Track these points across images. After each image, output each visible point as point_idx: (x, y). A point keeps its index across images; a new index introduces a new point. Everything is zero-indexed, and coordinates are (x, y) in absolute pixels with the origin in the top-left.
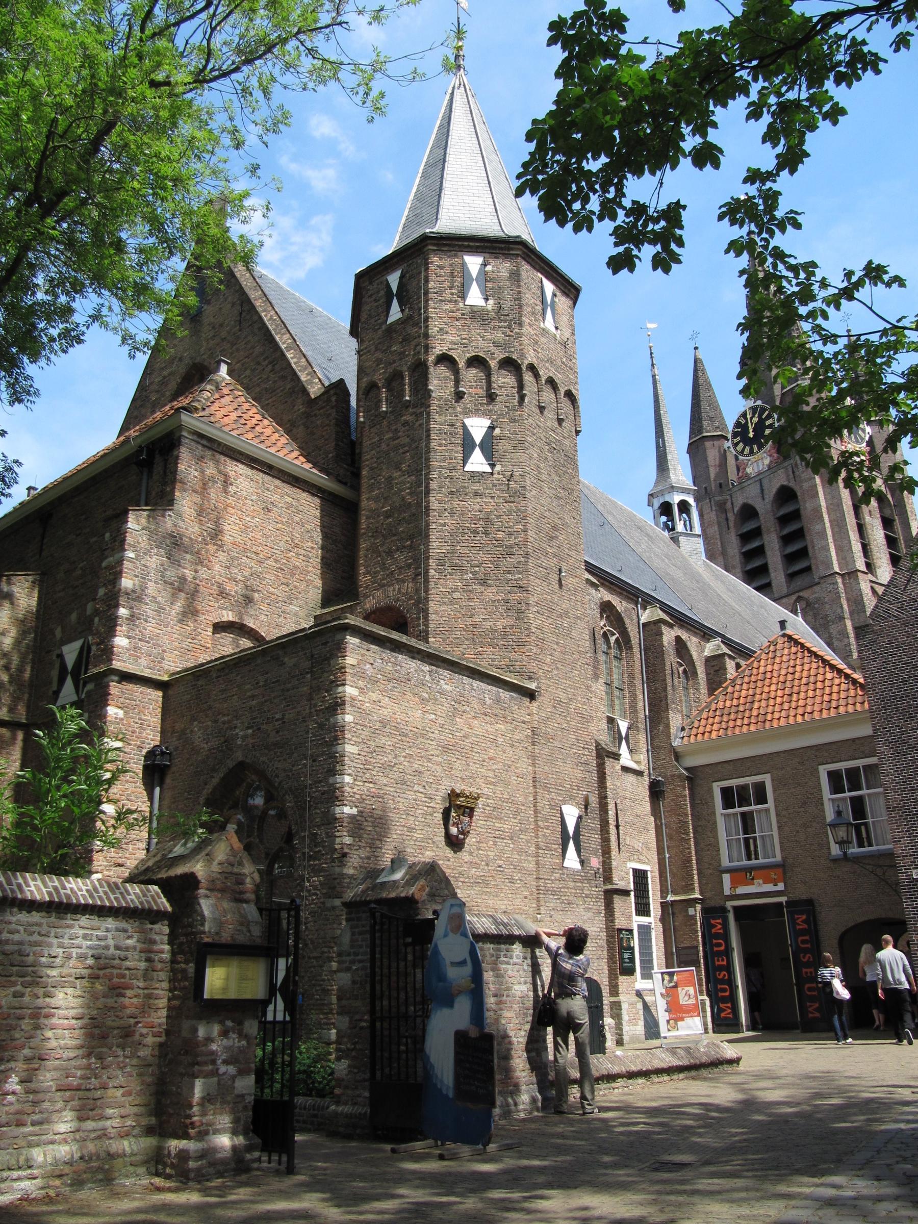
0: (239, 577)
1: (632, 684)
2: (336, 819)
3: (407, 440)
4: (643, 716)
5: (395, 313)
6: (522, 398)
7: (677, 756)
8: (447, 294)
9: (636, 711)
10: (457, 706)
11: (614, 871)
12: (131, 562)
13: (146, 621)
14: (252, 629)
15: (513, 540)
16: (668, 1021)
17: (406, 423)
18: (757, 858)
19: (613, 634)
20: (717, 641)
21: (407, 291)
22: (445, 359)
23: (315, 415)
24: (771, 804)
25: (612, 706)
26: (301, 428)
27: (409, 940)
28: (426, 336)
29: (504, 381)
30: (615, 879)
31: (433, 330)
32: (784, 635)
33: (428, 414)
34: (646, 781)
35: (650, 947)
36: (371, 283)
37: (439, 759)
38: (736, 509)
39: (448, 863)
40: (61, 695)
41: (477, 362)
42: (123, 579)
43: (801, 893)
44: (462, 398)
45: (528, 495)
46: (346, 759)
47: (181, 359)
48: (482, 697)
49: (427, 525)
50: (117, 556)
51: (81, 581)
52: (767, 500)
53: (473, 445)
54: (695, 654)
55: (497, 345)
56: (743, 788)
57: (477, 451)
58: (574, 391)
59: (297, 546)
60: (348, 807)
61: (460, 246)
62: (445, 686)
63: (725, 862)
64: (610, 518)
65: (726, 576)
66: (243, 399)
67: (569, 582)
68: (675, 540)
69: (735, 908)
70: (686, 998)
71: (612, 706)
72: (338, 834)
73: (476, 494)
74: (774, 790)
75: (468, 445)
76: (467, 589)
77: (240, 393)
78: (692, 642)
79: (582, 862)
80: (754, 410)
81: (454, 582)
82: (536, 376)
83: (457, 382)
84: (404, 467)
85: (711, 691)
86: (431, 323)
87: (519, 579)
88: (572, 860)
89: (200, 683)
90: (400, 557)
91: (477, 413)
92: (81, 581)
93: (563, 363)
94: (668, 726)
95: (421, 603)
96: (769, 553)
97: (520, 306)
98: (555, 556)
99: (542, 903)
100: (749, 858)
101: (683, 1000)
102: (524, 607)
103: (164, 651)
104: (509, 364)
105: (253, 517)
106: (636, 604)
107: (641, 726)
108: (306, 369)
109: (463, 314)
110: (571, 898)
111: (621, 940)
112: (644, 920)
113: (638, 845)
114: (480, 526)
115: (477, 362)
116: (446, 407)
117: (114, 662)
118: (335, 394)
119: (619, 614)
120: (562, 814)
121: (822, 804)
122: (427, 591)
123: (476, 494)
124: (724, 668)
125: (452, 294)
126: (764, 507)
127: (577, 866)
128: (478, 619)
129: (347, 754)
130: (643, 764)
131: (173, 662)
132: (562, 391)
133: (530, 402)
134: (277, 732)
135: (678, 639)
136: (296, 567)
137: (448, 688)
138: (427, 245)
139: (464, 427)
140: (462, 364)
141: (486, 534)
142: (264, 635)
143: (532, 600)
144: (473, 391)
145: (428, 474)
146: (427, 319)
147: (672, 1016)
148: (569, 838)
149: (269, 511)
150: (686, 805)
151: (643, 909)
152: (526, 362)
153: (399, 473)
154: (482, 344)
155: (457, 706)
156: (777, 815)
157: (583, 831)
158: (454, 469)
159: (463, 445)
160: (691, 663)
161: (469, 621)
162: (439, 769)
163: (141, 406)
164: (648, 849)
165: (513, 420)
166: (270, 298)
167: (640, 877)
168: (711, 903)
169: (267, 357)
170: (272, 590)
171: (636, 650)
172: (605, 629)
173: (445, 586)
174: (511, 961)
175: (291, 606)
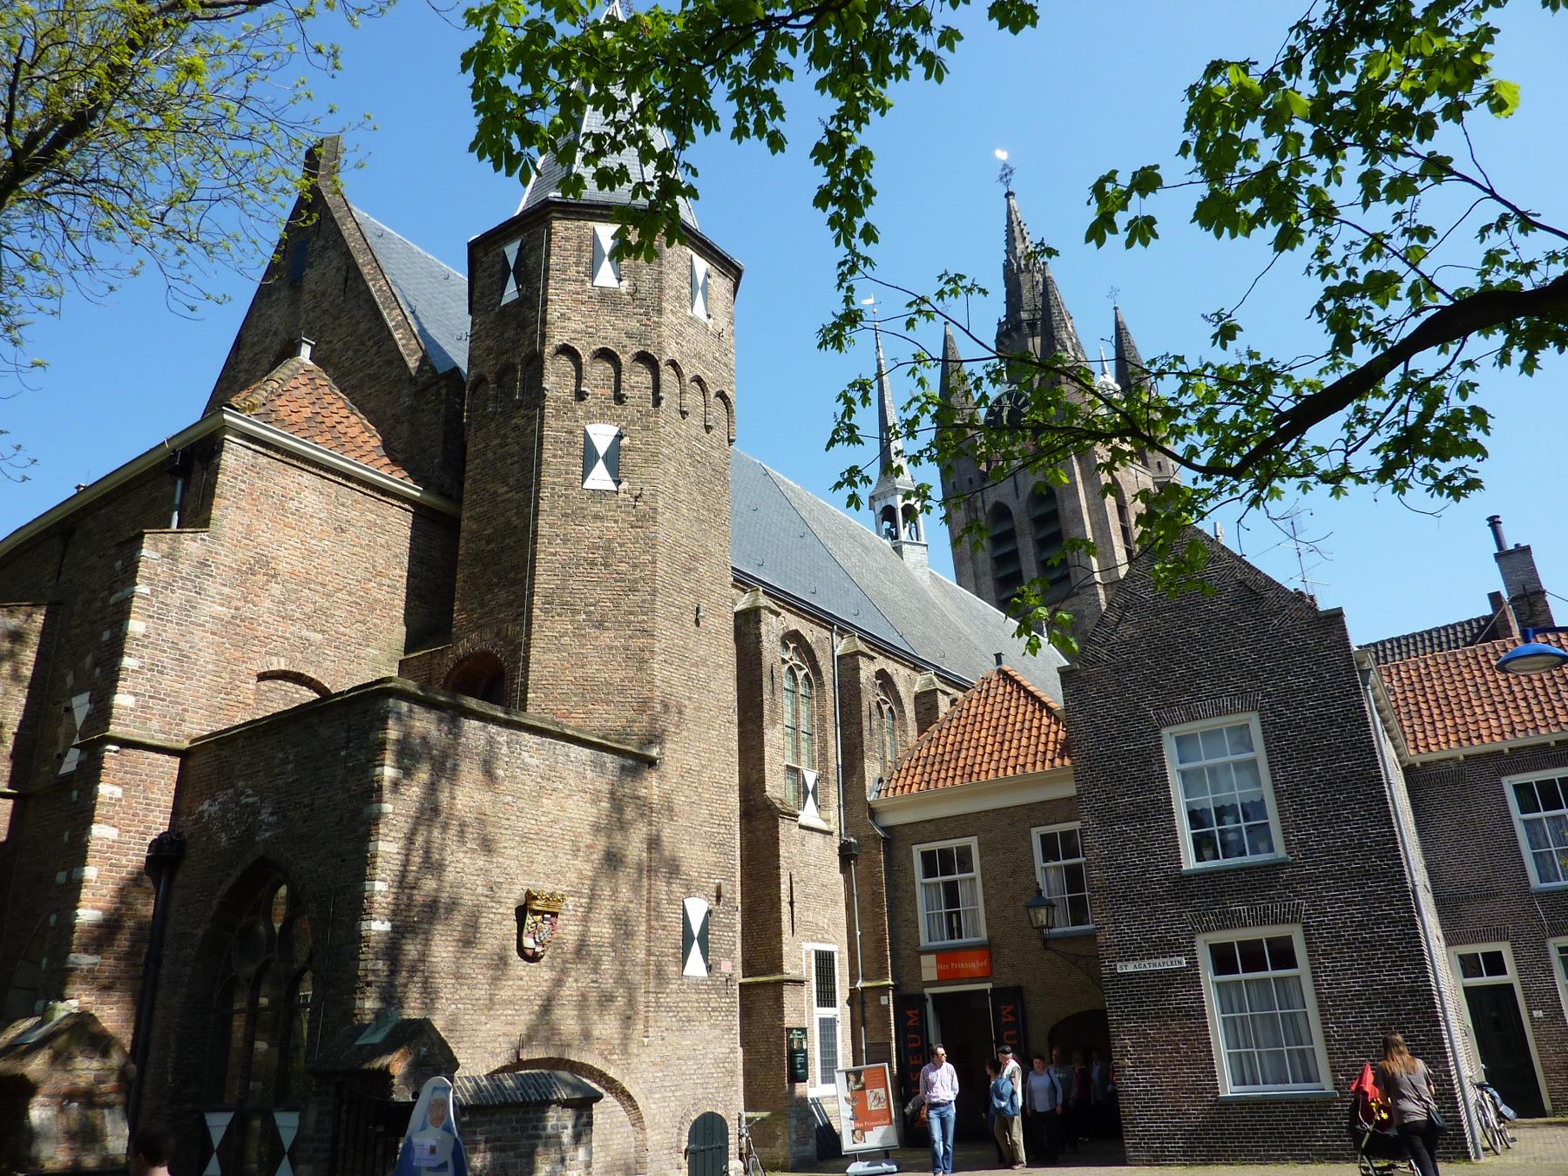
0: (297, 615)
1: (822, 729)
2: (361, 937)
3: (517, 448)
4: (834, 766)
5: (511, 292)
6: (657, 401)
7: (873, 813)
8: (572, 272)
9: (826, 760)
10: (544, 783)
11: (785, 958)
12: (144, 598)
13: (162, 673)
14: (312, 679)
15: (638, 574)
16: (853, 1132)
17: (517, 427)
18: (960, 937)
19: (801, 669)
20: (931, 674)
21: (525, 266)
22: (567, 351)
23: (423, 411)
24: (977, 872)
25: (797, 754)
26: (406, 425)
27: (380, 1129)
28: (544, 322)
29: (637, 380)
30: (786, 968)
31: (553, 313)
32: (1000, 671)
33: (542, 418)
34: (837, 842)
35: (835, 1045)
36: (486, 254)
37: (515, 852)
38: (987, 509)
39: (520, 983)
40: (66, 760)
41: (605, 355)
42: (131, 622)
43: (1008, 979)
44: (584, 399)
45: (659, 518)
46: (379, 860)
47: (275, 333)
48: (581, 770)
49: (534, 554)
50: (127, 591)
51: (99, 616)
52: (1021, 499)
53: (606, 459)
54: (902, 689)
55: (630, 336)
56: (945, 853)
57: (600, 465)
58: (728, 393)
59: (380, 574)
60: (378, 922)
61: (590, 214)
62: (528, 760)
63: (924, 941)
64: (815, 527)
65: (958, 591)
66: (327, 390)
67: (709, 622)
68: (898, 550)
69: (934, 996)
70: (876, 1102)
71: (797, 754)
72: (362, 957)
73: (596, 517)
74: (981, 857)
75: (589, 457)
76: (578, 634)
77: (324, 383)
78: (899, 673)
79: (709, 968)
80: (1009, 395)
81: (564, 625)
82: (679, 374)
83: (579, 379)
84: (511, 481)
85: (922, 730)
86: (550, 308)
87: (644, 621)
88: (696, 965)
89: (224, 753)
90: (503, 595)
91: (602, 418)
92: (99, 616)
93: (715, 358)
94: (863, 777)
95: (519, 650)
96: (1023, 558)
97: (661, 289)
98: (691, 591)
99: (651, 1023)
100: (952, 938)
101: (872, 1105)
102: (647, 655)
103: (185, 710)
104: (645, 358)
105: (321, 540)
106: (831, 631)
107: (832, 777)
108: (415, 353)
109: (590, 297)
110: (692, 1014)
111: (791, 1041)
112: (827, 1012)
113: (823, 922)
114: (598, 556)
115: (605, 355)
116: (563, 410)
117: (111, 727)
118: (446, 385)
119: (809, 646)
120: (684, 910)
121: (1034, 874)
122: (529, 634)
123: (596, 517)
124: (934, 707)
125: (578, 272)
126: (1017, 506)
127: (703, 972)
128: (590, 670)
129: (380, 853)
130: (833, 822)
131: (198, 724)
132: (712, 393)
133: (668, 407)
134: (305, 821)
135: (882, 674)
136: (377, 601)
137: (534, 762)
138: (550, 212)
139: (586, 435)
140: (585, 358)
141: (606, 565)
142: (327, 685)
143: (657, 647)
144: (599, 391)
145: (538, 492)
146: (545, 302)
147: (858, 1125)
148: (693, 939)
149: (343, 531)
150: (880, 872)
151: (826, 997)
152: (665, 358)
153: (506, 489)
154: (612, 334)
155: (544, 783)
156: (984, 886)
157: (713, 929)
158: (570, 486)
159: (584, 458)
160: (898, 701)
161: (579, 674)
162: (514, 864)
163: (227, 388)
164: (836, 925)
165: (646, 428)
166: (382, 263)
167: (825, 962)
168: (910, 990)
169: (373, 337)
170: (342, 629)
171: (829, 687)
172: (791, 663)
173: (552, 629)
174: (543, 1133)
175: (368, 649)
